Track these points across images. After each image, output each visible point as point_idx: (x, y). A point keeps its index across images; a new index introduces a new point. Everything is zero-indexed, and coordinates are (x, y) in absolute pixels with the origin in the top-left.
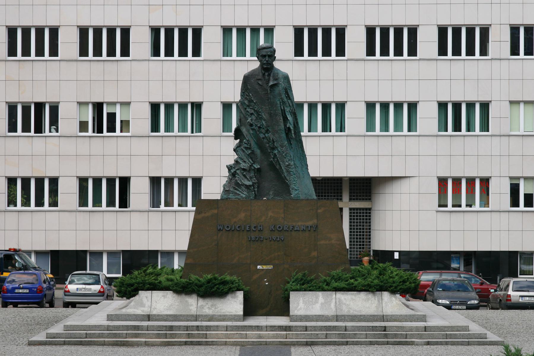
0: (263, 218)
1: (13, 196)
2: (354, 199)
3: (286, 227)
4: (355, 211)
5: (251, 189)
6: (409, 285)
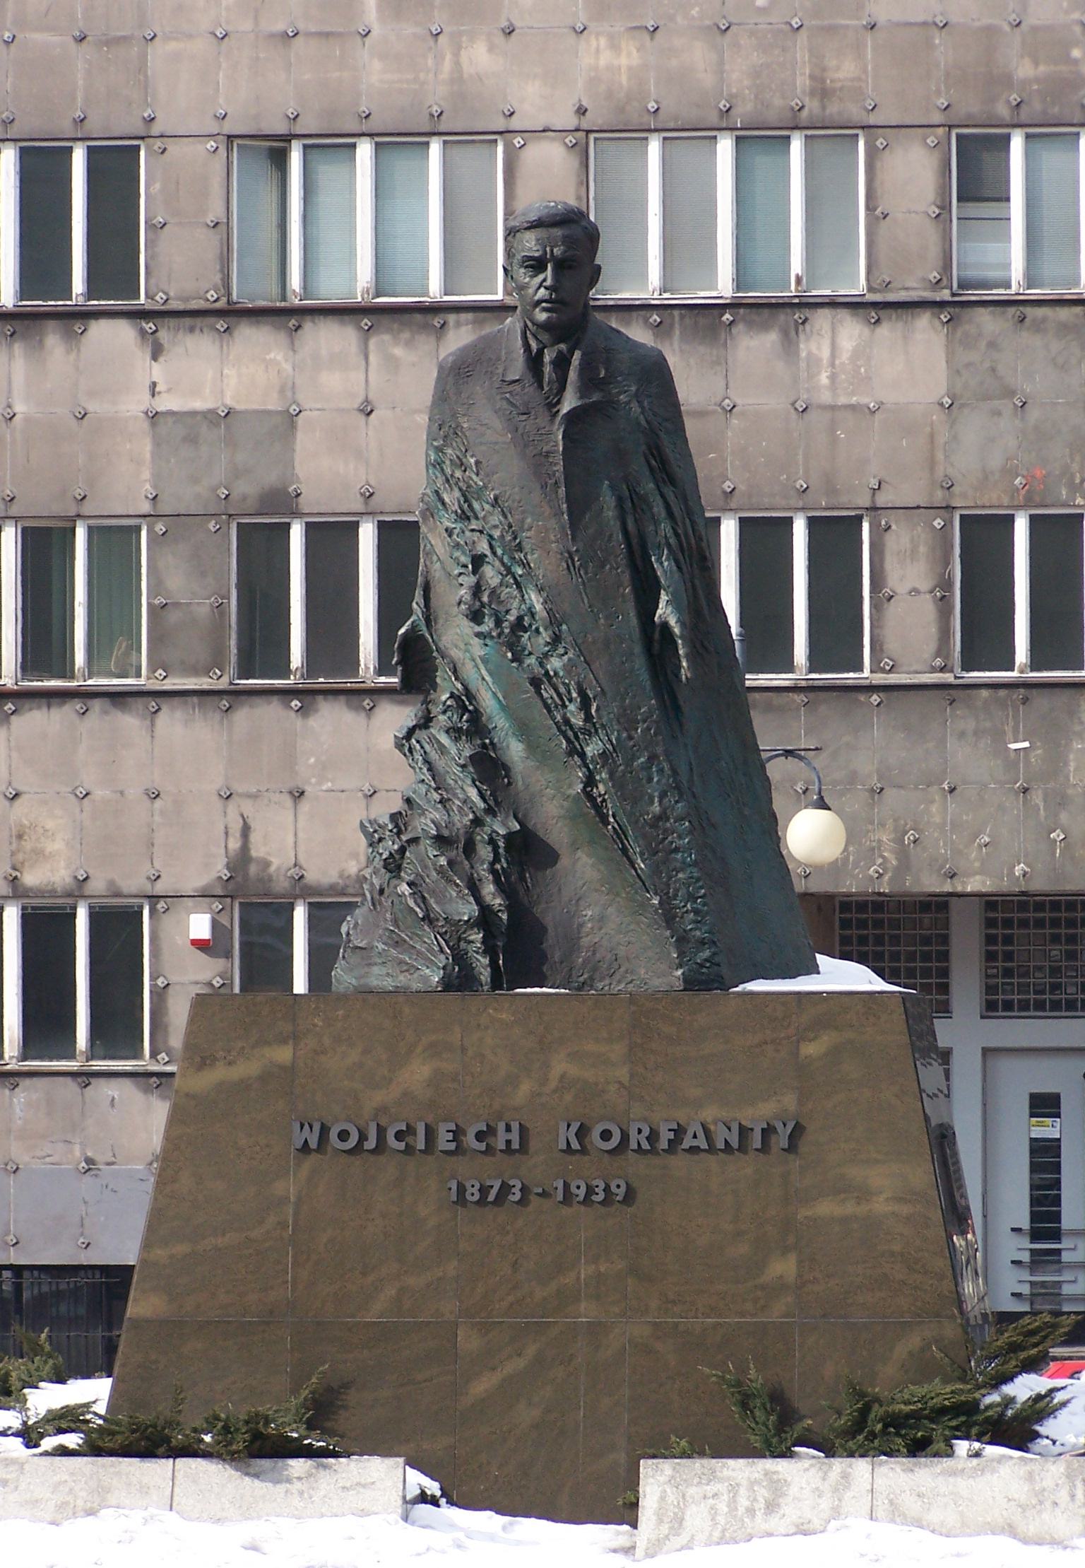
0: (525, 1088)
1: (973, 1364)
2: (1008, 1006)
3: (640, 1131)
4: (935, 964)
5: (473, 942)
6: (760, 20)
